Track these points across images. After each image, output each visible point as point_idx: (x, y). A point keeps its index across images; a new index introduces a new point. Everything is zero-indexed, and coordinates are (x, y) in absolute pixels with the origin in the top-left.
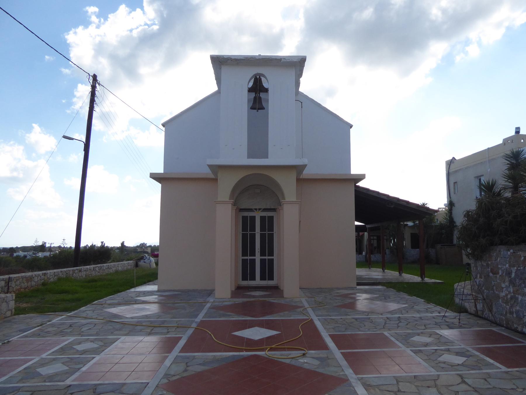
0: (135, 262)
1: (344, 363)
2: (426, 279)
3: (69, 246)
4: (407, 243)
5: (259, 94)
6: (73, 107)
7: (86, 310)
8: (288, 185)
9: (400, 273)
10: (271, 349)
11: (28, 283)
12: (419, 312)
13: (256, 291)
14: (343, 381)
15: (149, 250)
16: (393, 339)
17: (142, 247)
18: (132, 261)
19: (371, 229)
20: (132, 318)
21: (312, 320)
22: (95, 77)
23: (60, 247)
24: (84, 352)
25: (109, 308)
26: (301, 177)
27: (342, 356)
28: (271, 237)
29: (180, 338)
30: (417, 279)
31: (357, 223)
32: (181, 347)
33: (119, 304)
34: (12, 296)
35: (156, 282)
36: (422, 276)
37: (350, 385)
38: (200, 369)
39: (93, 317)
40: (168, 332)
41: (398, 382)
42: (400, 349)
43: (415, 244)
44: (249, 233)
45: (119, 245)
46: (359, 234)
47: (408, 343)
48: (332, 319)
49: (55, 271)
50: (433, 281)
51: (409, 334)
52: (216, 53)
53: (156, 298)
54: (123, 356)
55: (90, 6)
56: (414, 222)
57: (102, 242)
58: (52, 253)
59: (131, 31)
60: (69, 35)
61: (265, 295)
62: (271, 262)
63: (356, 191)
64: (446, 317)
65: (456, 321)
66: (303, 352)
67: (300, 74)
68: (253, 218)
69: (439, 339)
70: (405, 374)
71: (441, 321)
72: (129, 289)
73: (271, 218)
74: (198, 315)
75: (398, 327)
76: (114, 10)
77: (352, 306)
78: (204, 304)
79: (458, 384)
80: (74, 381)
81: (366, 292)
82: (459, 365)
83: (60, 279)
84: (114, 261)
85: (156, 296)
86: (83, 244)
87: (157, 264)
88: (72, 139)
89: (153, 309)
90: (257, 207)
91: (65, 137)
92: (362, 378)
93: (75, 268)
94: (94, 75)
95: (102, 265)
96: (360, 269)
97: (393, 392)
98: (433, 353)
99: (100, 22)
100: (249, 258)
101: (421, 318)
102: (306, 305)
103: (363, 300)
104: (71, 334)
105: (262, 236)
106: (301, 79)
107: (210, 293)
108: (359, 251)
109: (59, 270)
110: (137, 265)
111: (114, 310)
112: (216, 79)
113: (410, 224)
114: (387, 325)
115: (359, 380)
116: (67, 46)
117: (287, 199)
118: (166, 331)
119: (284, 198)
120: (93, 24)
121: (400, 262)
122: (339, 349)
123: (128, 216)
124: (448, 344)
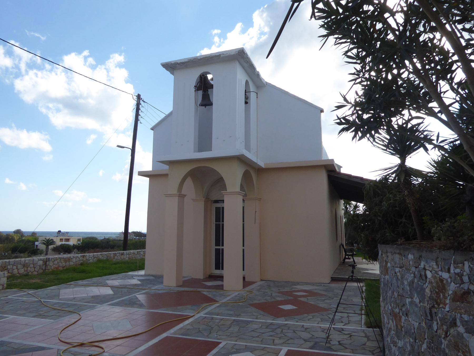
8: (233, 178)
11: (66, 263)
34: (4, 274)
86: (130, 230)
88: (124, 147)
94: (138, 94)
99: (220, 41)
117: (229, 190)
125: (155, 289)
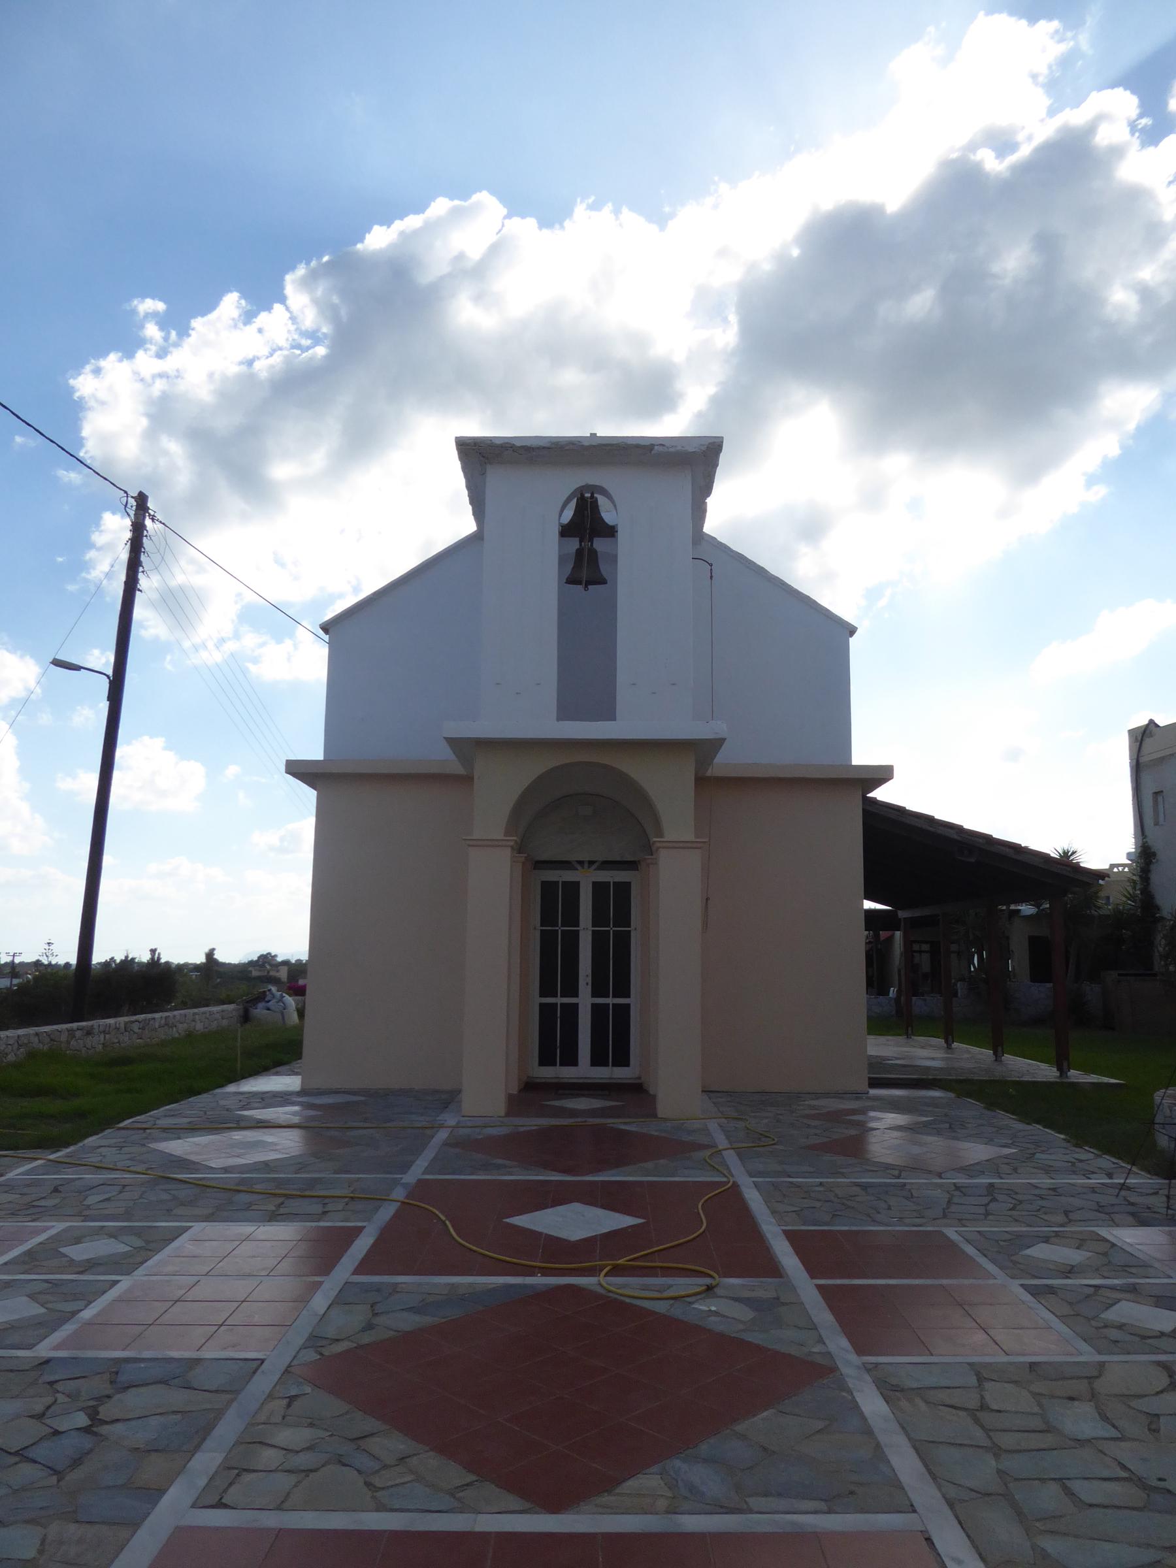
0: (241, 1007)
1: (823, 1317)
2: (1072, 1072)
3: (62, 962)
4: (1018, 963)
5: (591, 540)
6: (84, 574)
7: (100, 1145)
8: (671, 797)
9: (995, 1053)
10: (616, 1271)
12: (1048, 1170)
13: (578, 1096)
14: (820, 1371)
15: (283, 974)
16: (970, 1250)
17: (263, 966)
18: (232, 1007)
19: (914, 923)
20: (226, 1170)
21: (735, 1186)
22: (142, 499)
23: (37, 963)
24: (91, 1265)
25: (166, 1139)
26: (709, 773)
27: (820, 1299)
28: (623, 942)
29: (360, 1230)
30: (1046, 1072)
31: (868, 905)
32: (360, 1257)
33: (193, 1129)
35: (296, 1065)
36: (1062, 1062)
37: (842, 1386)
38: (408, 1322)
39: (120, 1165)
40: (325, 1213)
41: (981, 1379)
42: (991, 1282)
43: (1041, 970)
44: (560, 929)
45: (200, 959)
46: (877, 936)
47: (1015, 1263)
48: (798, 1186)
49: (21, 1032)
50: (1094, 1078)
51: (1019, 1236)
52: (475, 428)
53: (294, 1114)
54: (196, 1279)
55: (143, 296)
56: (1038, 907)
57: (153, 951)
58: (15, 981)
59: (250, 363)
60: (81, 378)
61: (603, 1109)
62: (623, 1013)
63: (866, 813)
64: (1129, 1189)
65: (1158, 1202)
66: (708, 1281)
67: (706, 488)
68: (572, 889)
69: (1105, 1254)
70: (1005, 1359)
71: (1114, 1200)
72: (222, 1086)
73: (624, 890)
74: (412, 1163)
75: (987, 1214)
76: (208, 305)
77: (853, 1146)
78: (428, 1132)
79: (1158, 1393)
80: (57, 1348)
81: (895, 1106)
82: (1162, 1334)
83: (32, 1055)
84: (184, 1005)
85: (297, 1108)
86: (99, 956)
87: (301, 1013)
88: (77, 668)
89: (286, 1144)
90: (586, 857)
91: (57, 663)
92: (877, 1365)
93: (75, 1025)
95: (150, 1016)
96: (882, 1039)
97: (965, 1409)
98: (1088, 1296)
99: (166, 339)
100: (560, 1000)
101: (1054, 1189)
102: (722, 1141)
103: (887, 1130)
104: (54, 1213)
105: (599, 941)
106: (708, 500)
107: (448, 1099)
108: (876, 982)
109: (32, 1030)
110: (246, 1018)
111: (177, 1147)
112: (471, 503)
113: (1027, 909)
114: (953, 1208)
115: (868, 1371)
116: (74, 409)
117: (670, 835)
118: (317, 1208)
119: (660, 834)
120: (148, 346)
121: (998, 1024)
122: (812, 1277)
123: (227, 878)
124: (1134, 1270)
125: (36, 1159)
